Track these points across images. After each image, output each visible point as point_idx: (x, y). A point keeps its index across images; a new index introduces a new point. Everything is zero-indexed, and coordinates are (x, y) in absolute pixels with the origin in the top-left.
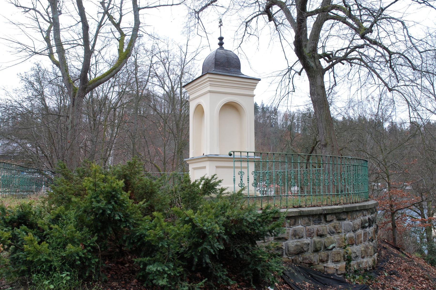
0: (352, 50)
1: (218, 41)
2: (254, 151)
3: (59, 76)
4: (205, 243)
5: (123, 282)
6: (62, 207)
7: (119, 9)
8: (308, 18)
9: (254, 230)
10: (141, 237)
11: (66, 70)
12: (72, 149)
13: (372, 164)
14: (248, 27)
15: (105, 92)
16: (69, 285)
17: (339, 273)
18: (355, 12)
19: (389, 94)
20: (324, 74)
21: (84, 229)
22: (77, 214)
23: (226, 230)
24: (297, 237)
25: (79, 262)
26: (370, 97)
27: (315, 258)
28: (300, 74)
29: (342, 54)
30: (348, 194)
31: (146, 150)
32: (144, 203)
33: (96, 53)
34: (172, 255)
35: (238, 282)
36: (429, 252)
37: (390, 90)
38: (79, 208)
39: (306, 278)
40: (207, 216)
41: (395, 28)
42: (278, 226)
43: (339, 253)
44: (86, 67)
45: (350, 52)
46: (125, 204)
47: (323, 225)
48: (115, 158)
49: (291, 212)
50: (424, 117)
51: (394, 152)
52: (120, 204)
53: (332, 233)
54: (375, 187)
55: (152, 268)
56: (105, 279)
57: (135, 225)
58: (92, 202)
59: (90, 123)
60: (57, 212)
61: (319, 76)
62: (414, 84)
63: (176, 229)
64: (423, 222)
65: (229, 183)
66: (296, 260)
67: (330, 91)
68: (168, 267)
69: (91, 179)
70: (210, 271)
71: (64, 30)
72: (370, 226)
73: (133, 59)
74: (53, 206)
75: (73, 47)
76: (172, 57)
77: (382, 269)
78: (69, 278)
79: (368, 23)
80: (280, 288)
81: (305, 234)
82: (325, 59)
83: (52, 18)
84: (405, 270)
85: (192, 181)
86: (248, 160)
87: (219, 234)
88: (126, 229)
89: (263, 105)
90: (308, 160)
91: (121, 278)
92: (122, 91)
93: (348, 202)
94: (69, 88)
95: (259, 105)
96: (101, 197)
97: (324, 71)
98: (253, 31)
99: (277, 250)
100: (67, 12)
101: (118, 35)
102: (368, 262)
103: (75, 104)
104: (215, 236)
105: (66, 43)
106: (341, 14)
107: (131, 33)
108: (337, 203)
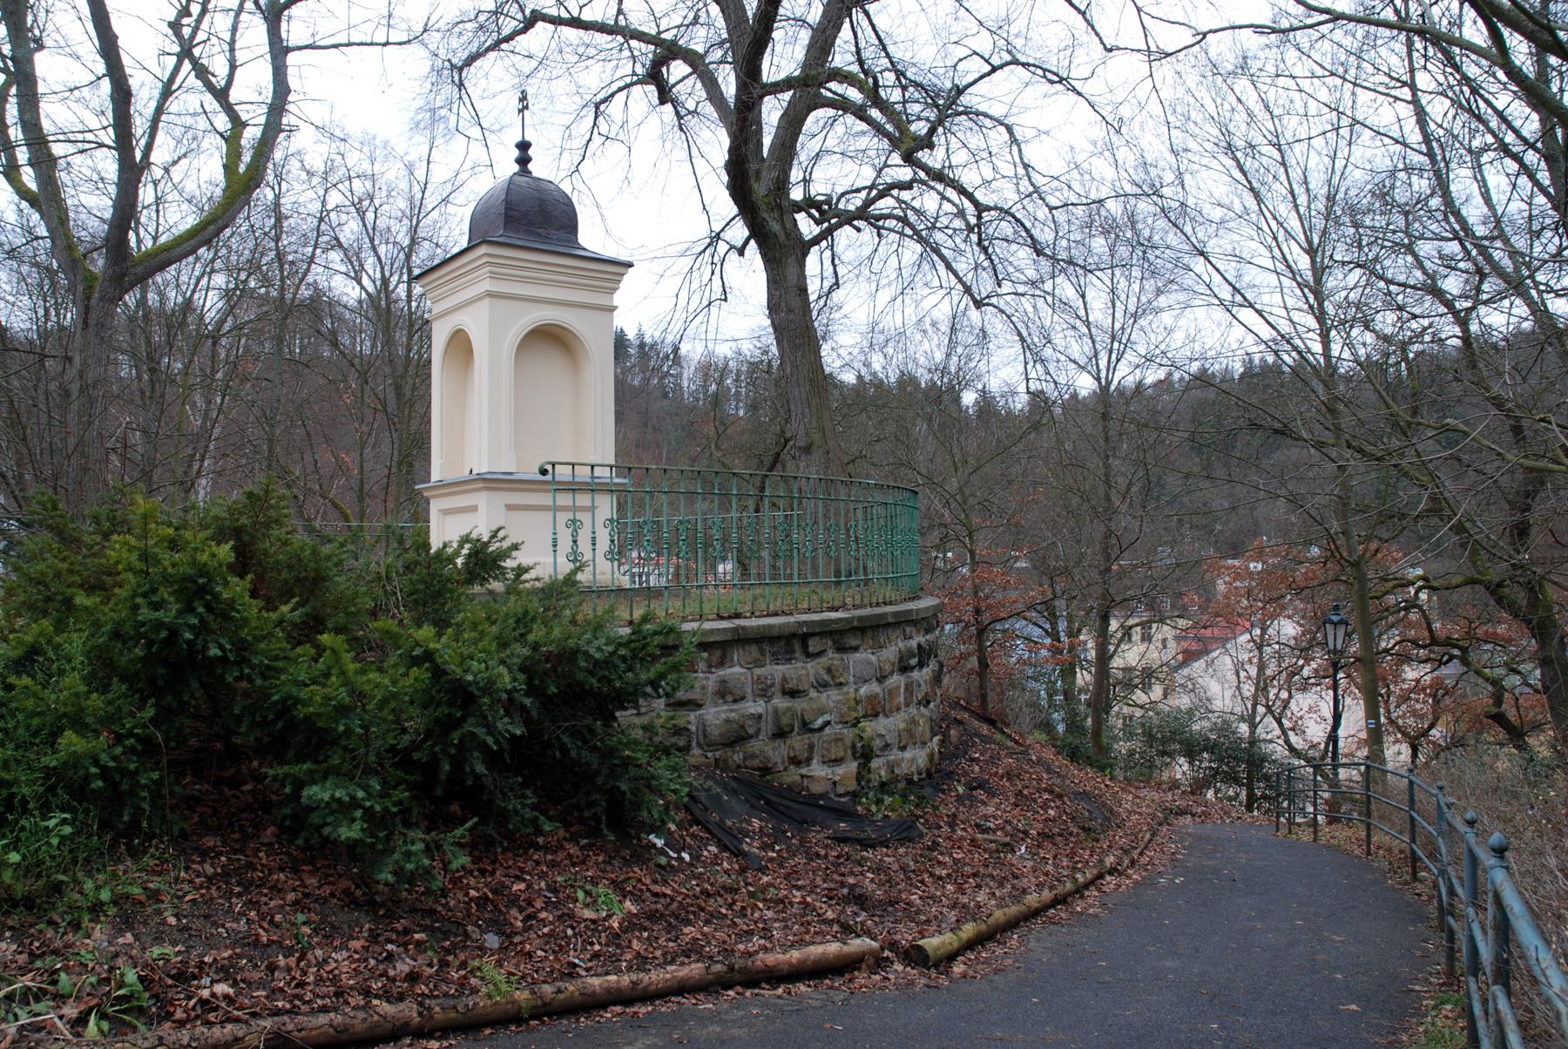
0: (881, 195)
1: (516, 153)
2: (613, 462)
3: (37, 238)
4: (471, 720)
5: (236, 836)
6: (45, 623)
7: (226, 47)
8: (766, 99)
9: (610, 681)
10: (286, 707)
11: (60, 218)
12: (82, 454)
13: (930, 500)
14: (601, 119)
15: (184, 288)
16: (71, 851)
17: (841, 790)
18: (889, 90)
19: (974, 314)
20: (805, 254)
21: (114, 687)
22: (94, 642)
23: (529, 683)
24: (729, 698)
25: (100, 783)
26: (928, 320)
27: (776, 753)
28: (741, 252)
29: (855, 202)
30: (866, 582)
31: (308, 458)
32: (293, 610)
33: (158, 173)
34: (378, 755)
35: (567, 825)
36: (1069, 729)
37: (978, 304)
38: (97, 624)
39: (752, 806)
40: (475, 644)
41: (991, 143)
42: (676, 668)
43: (839, 740)
44: (126, 211)
45: (873, 201)
46: (238, 611)
47: (800, 664)
48: (215, 483)
49: (712, 631)
50: (1062, 380)
51: (987, 469)
52: (223, 612)
53: (822, 686)
54: (940, 564)
55: (318, 793)
56: (182, 829)
57: (269, 672)
58: (136, 607)
59: (139, 377)
60: (29, 639)
61: (791, 261)
62: (1038, 292)
63: (387, 681)
64: (1056, 651)
65: (540, 553)
66: (726, 761)
67: (822, 302)
68: (366, 788)
69: (133, 541)
70: (485, 797)
71: (54, 98)
72: (921, 665)
73: (270, 196)
74: (20, 622)
75: (81, 152)
76: (384, 193)
77: (950, 775)
78: (68, 830)
79: (922, 123)
80: (681, 836)
81: (749, 690)
82: (811, 216)
83: (12, 59)
84: (1009, 775)
85: (435, 544)
86: (593, 488)
87: (509, 692)
88: (244, 684)
89: (641, 336)
90: (762, 489)
91: (231, 824)
92: (237, 288)
93: (866, 601)
94: (70, 275)
95: (631, 334)
96: (164, 593)
97: (805, 247)
98: (615, 128)
99: (675, 734)
100: (63, 44)
101: (222, 122)
102: (915, 758)
103: (92, 322)
104: (499, 700)
105: (62, 137)
106: (854, 94)
107: (262, 119)
108: (837, 603)
